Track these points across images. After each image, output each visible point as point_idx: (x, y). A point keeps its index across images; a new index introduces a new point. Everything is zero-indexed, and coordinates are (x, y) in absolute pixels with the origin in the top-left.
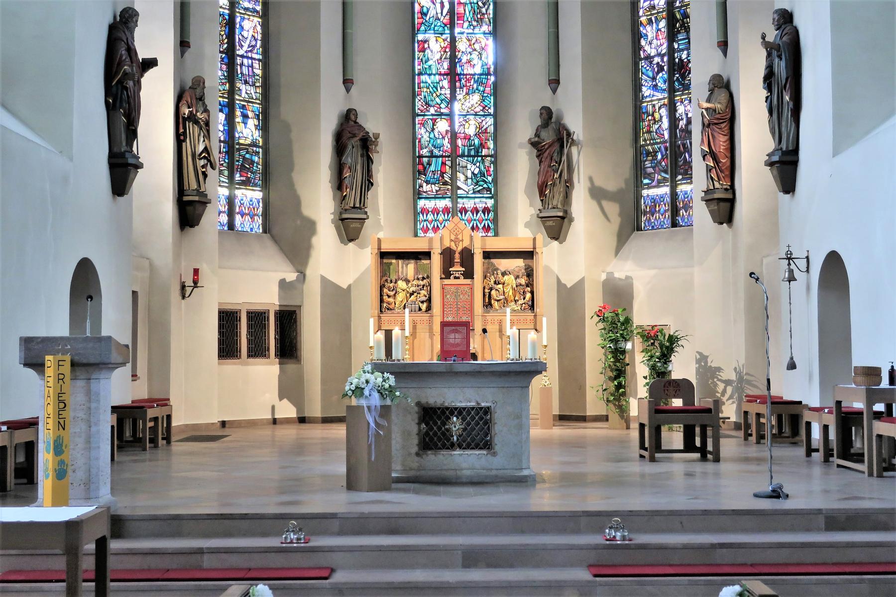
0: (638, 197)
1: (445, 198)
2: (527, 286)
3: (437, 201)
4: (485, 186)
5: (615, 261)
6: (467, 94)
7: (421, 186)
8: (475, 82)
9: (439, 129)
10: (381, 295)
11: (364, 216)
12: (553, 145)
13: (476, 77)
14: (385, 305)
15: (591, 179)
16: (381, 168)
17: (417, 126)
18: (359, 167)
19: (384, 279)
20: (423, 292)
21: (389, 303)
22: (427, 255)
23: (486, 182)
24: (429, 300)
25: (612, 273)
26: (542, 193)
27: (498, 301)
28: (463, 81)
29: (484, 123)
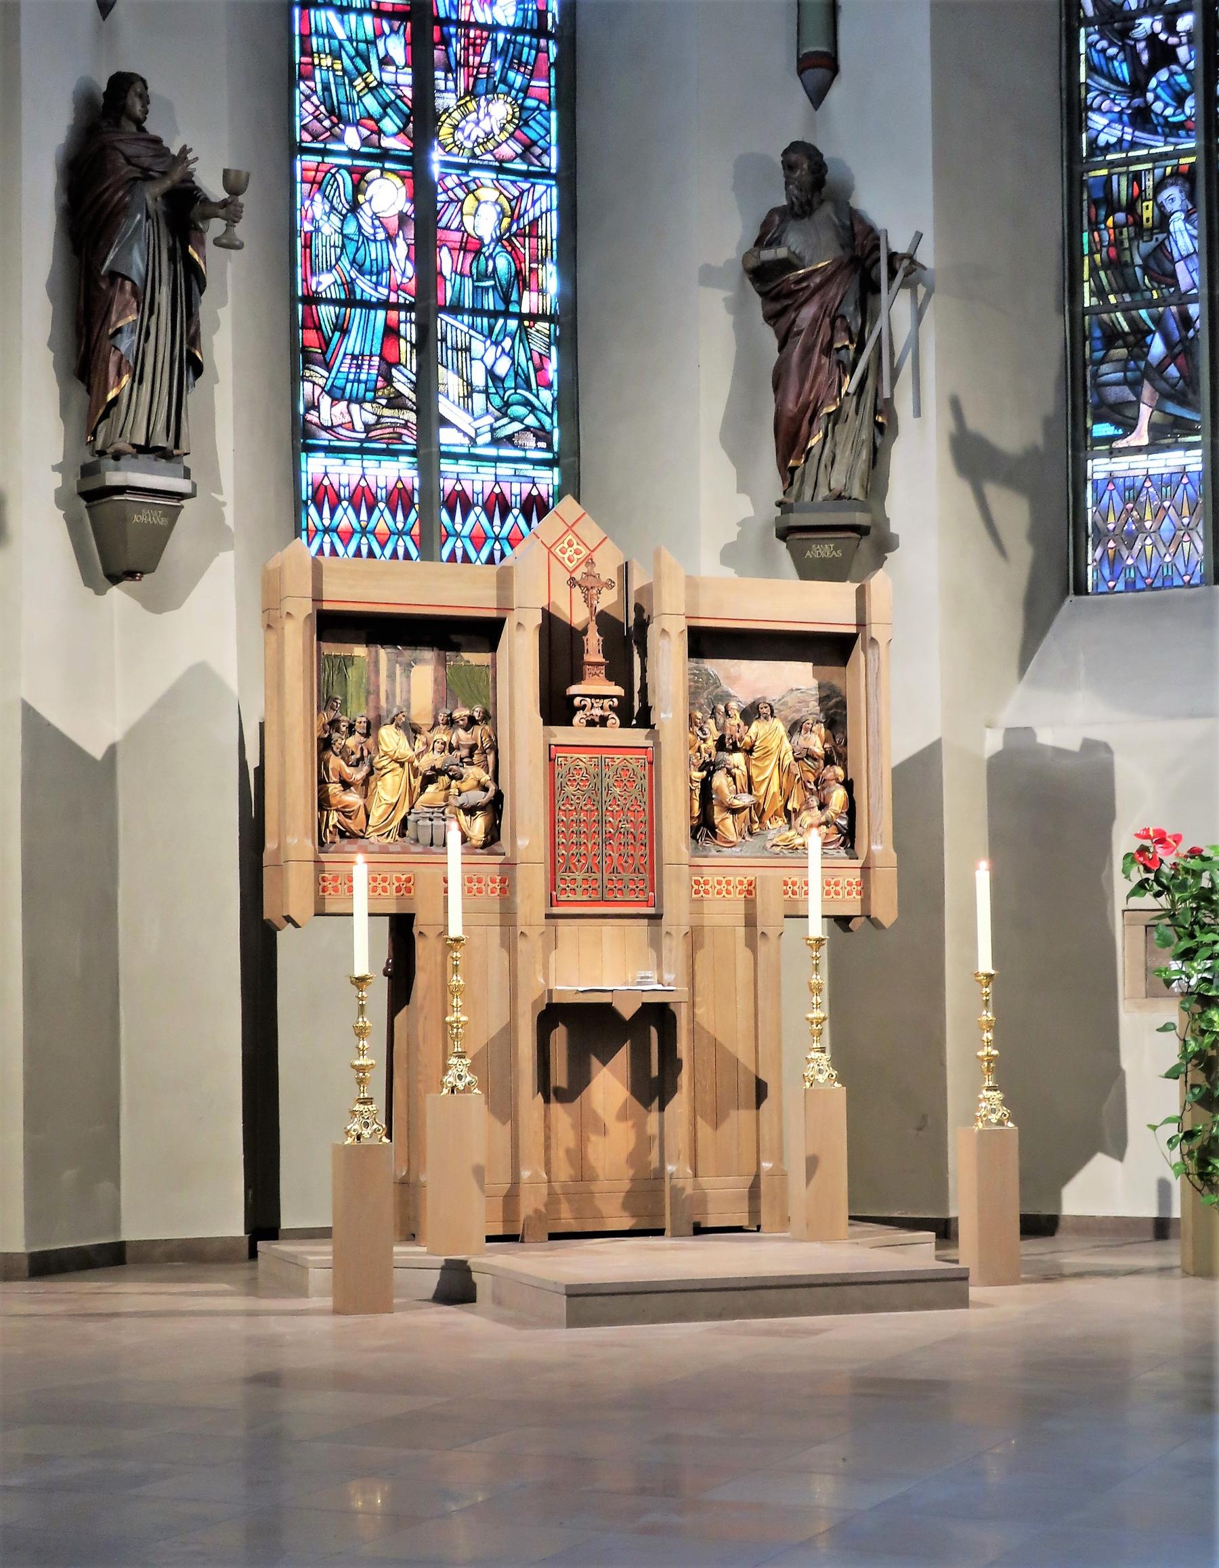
0: (1079, 479)
1: (395, 454)
2: (828, 760)
3: (370, 462)
4: (531, 421)
5: (1020, 692)
6: (471, 93)
7: (313, 406)
8: (495, 54)
9: (377, 206)
10: (322, 782)
11: (181, 485)
12: (820, 284)
13: (501, 37)
14: (334, 818)
15: (956, 407)
16: (225, 315)
17: (302, 189)
18: (164, 297)
19: (327, 717)
20: (474, 773)
21: (346, 812)
22: (485, 632)
23: (533, 409)
24: (495, 807)
25: (1029, 731)
26: (790, 441)
27: (735, 811)
28: (456, 47)
29: (526, 201)
